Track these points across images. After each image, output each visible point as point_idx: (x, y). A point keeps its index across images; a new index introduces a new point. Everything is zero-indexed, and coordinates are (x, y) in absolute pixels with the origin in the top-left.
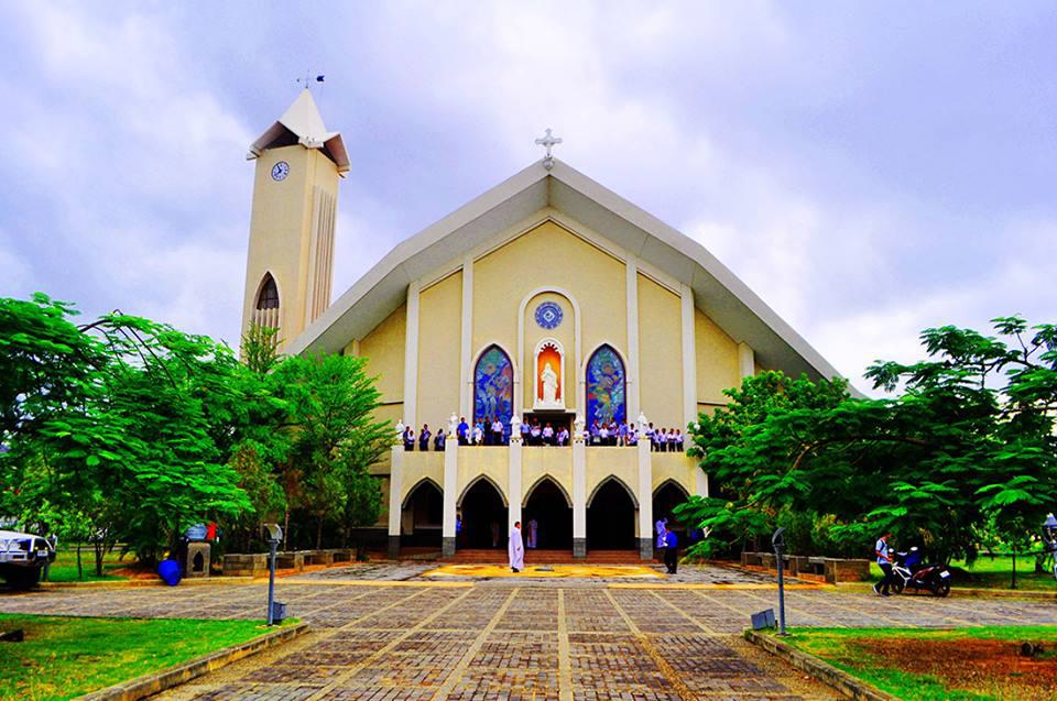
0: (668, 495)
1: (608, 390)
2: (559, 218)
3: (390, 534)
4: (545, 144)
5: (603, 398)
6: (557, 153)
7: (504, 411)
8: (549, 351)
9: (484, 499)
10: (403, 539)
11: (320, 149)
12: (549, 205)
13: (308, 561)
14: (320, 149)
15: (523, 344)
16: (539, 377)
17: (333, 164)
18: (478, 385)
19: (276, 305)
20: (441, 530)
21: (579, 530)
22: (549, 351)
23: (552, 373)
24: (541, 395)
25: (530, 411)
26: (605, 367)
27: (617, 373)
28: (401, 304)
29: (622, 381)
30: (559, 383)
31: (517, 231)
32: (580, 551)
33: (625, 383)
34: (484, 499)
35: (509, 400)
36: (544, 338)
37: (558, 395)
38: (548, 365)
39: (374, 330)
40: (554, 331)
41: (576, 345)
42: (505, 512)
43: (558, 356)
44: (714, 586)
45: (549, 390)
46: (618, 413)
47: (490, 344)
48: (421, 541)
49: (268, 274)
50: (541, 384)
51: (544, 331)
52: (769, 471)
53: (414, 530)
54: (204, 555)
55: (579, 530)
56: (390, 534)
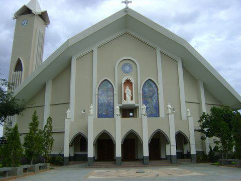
0: (181, 139)
2: (129, 32)
3: (65, 156)
4: (125, 3)
6: (130, 6)
8: (128, 82)
9: (132, 141)
10: (70, 158)
12: (126, 28)
13: (25, 170)
15: (118, 79)
16: (124, 91)
17: (43, 21)
19: (22, 70)
20: (87, 154)
22: (128, 82)
23: (130, 90)
24: (125, 99)
26: (150, 90)
28: (68, 66)
30: (132, 94)
33: (158, 94)
34: (132, 141)
35: (112, 101)
37: (132, 99)
39: (58, 75)
41: (139, 81)
43: (131, 83)
44: (44, 126)
45: (128, 97)
47: (103, 79)
48: (79, 157)
49: (19, 59)
50: (125, 94)
56: (65, 156)
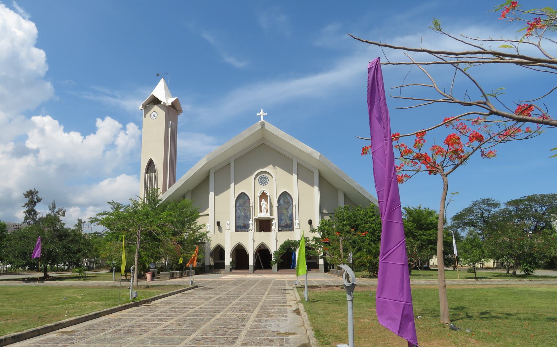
1: (287, 209)
5: (284, 211)
7: (247, 217)
11: (113, 142)
14: (113, 142)
18: (237, 208)
20: (224, 263)
21: (251, 262)
24: (261, 211)
25: (257, 217)
27: (289, 202)
29: (291, 205)
31: (522, 29)
32: (275, 267)
36: (260, 189)
38: (263, 200)
40: (265, 186)
42: (247, 256)
43: (267, 196)
46: (290, 217)
50: (261, 207)
51: (262, 186)
52: (199, 252)
53: (215, 263)
54: (155, 272)
55: (251, 262)
